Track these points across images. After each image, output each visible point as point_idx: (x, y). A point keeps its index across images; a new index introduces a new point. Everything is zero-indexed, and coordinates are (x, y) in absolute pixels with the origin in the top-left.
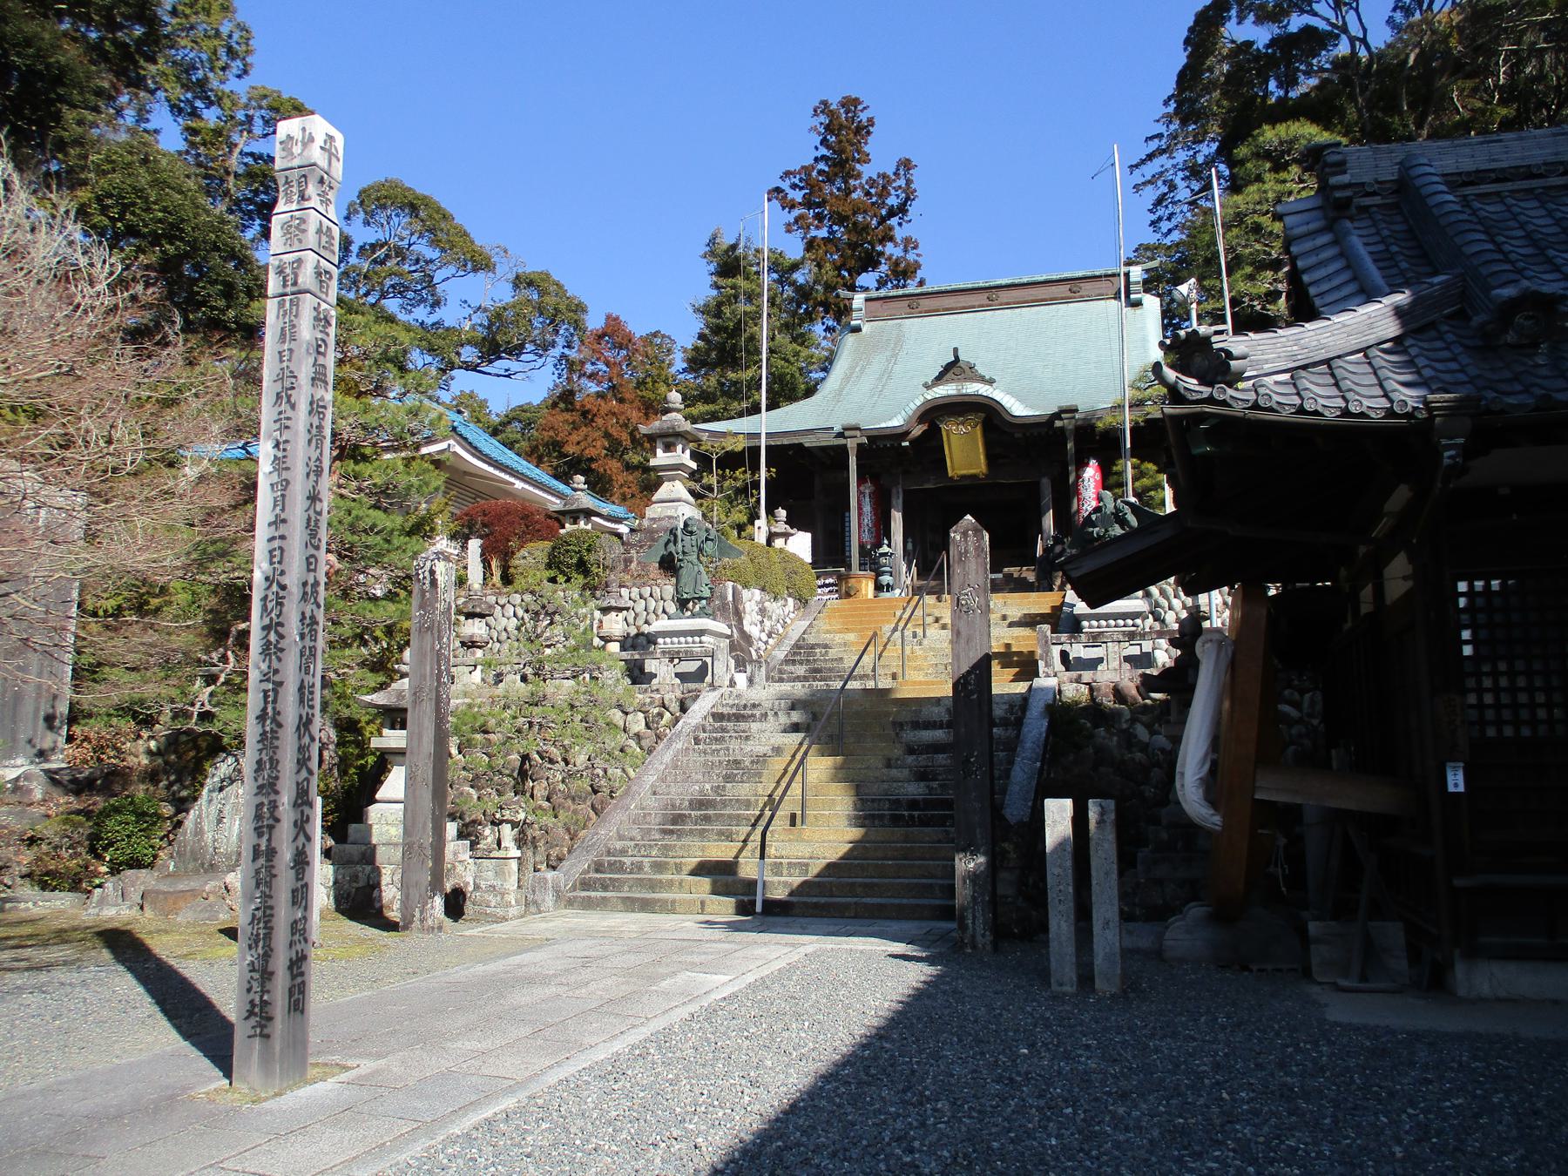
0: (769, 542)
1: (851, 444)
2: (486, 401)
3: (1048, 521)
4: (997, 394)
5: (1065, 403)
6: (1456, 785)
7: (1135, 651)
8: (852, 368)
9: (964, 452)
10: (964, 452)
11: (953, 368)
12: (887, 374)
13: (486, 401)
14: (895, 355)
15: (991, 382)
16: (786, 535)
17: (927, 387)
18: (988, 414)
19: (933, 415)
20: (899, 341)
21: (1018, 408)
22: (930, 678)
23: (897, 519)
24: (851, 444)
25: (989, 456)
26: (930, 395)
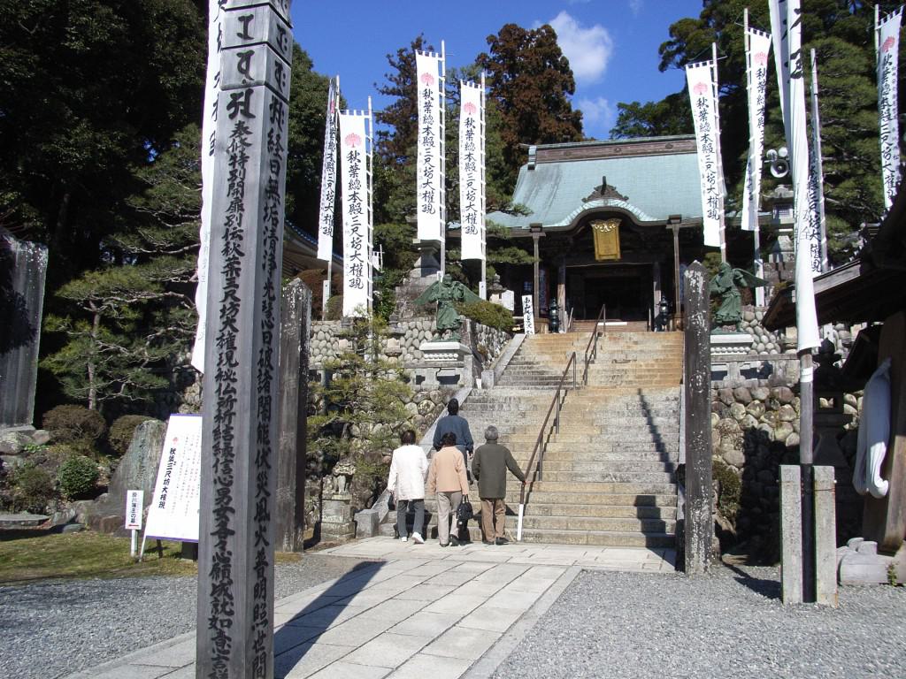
0: (488, 298)
1: (536, 236)
2: (214, 512)
3: (658, 296)
4: (630, 208)
5: (677, 213)
6: (134, 495)
7: (747, 367)
8: (530, 191)
9: (607, 242)
10: (607, 242)
11: (604, 190)
12: (553, 195)
13: (214, 512)
14: (557, 184)
15: (626, 199)
16: (500, 292)
17: (585, 201)
18: (625, 220)
19: (588, 219)
20: (559, 176)
21: (645, 218)
22: (603, 385)
23: (562, 289)
24: (536, 236)
25: (622, 248)
26: (587, 206)
